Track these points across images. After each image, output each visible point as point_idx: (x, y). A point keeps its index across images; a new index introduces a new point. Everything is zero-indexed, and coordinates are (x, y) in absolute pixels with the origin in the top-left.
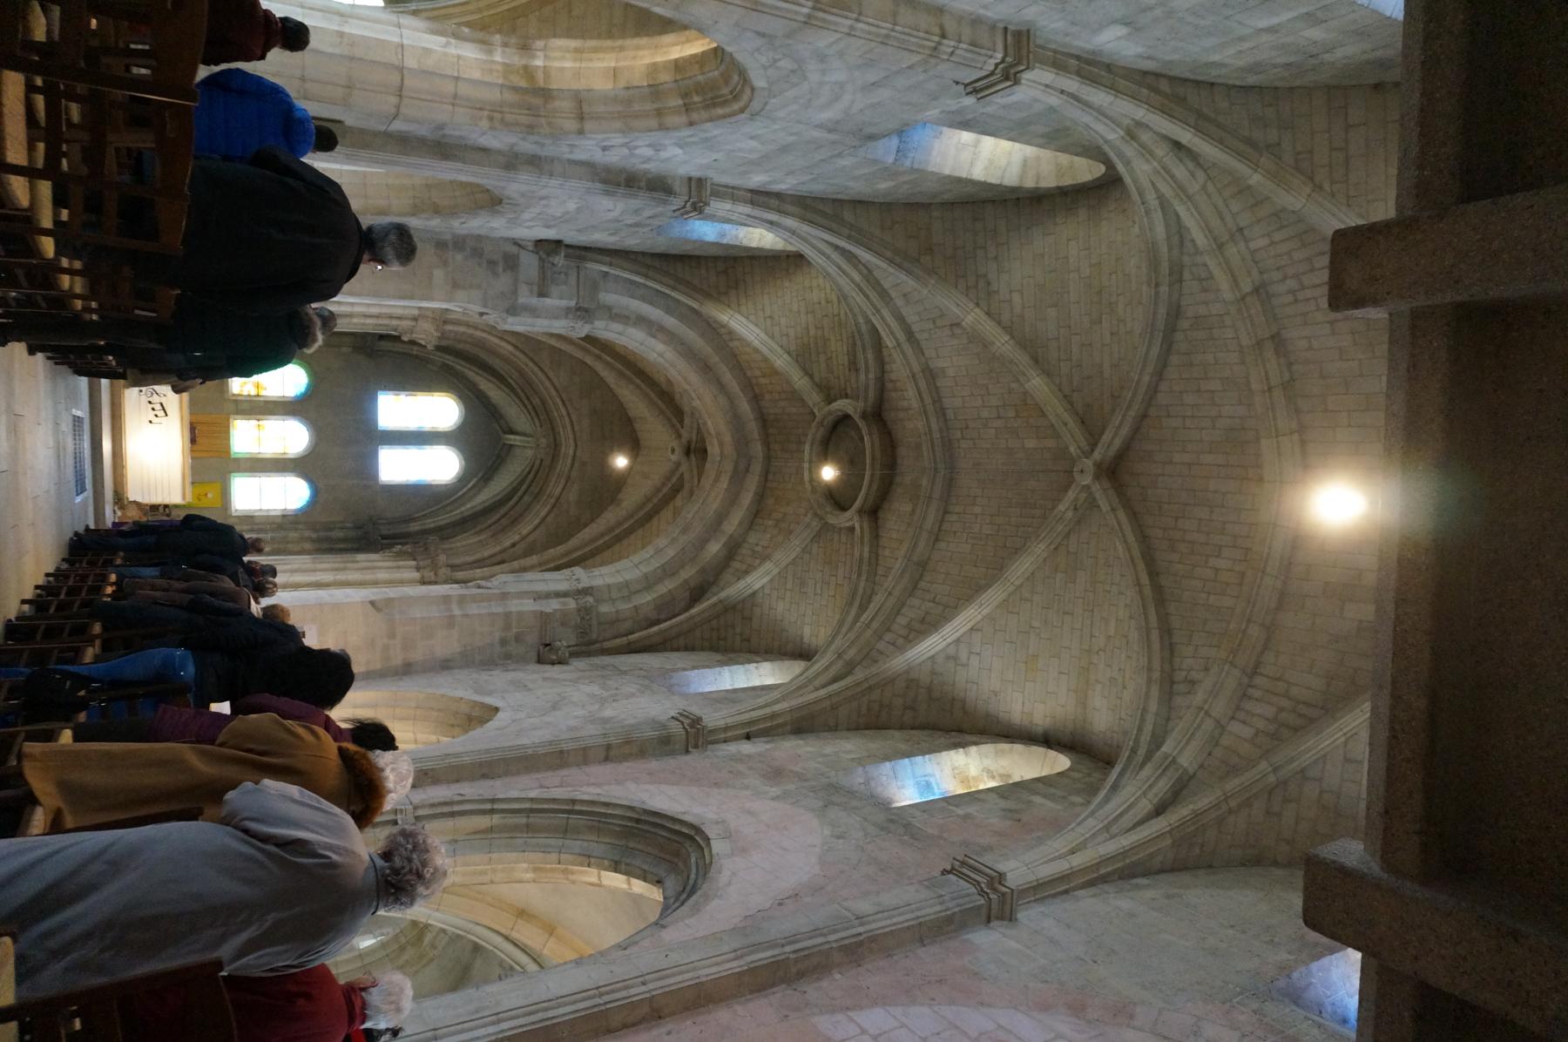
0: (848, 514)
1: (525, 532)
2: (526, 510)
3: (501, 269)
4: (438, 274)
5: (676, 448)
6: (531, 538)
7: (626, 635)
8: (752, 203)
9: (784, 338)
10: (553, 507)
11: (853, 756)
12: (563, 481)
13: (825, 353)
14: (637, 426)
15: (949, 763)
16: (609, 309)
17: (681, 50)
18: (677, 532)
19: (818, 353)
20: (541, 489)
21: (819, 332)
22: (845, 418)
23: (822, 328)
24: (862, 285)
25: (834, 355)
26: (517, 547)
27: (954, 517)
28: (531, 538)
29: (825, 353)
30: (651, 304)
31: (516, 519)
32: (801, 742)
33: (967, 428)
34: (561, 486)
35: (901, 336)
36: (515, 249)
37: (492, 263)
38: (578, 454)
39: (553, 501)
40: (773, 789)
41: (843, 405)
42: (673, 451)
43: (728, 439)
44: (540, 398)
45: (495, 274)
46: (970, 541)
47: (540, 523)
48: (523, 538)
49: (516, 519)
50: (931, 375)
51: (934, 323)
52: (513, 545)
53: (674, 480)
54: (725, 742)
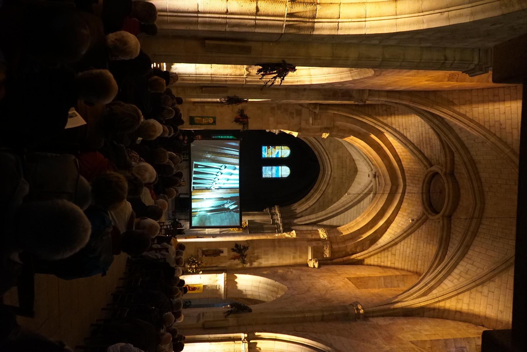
0: (438, 216)
1: (311, 204)
2: (312, 195)
3: (295, 116)
4: (272, 119)
5: (370, 175)
6: (313, 207)
7: (342, 257)
8: (387, 96)
9: (412, 137)
10: (322, 195)
11: (427, 333)
12: (326, 185)
13: (430, 144)
14: (356, 162)
15: (474, 342)
16: (338, 127)
17: (290, 133)
18: (365, 215)
19: (427, 144)
20: (318, 187)
21: (427, 135)
22: (436, 174)
23: (429, 133)
24: (439, 125)
25: (434, 145)
26: (308, 210)
27: (484, 227)
28: (313, 207)
29: (430, 144)
30: (355, 124)
31: (308, 199)
32: (405, 322)
33: (491, 187)
34: (325, 186)
35: (459, 147)
36: (300, 107)
37: (291, 113)
38: (332, 174)
39: (322, 192)
40: (387, 347)
41: (434, 168)
42: (369, 176)
43: (388, 178)
44: (318, 152)
45: (293, 118)
46: (492, 239)
47: (317, 201)
48: (310, 207)
49: (308, 199)
50: (472, 162)
51: (474, 141)
52: (306, 210)
53: (370, 187)
54: (373, 317)
